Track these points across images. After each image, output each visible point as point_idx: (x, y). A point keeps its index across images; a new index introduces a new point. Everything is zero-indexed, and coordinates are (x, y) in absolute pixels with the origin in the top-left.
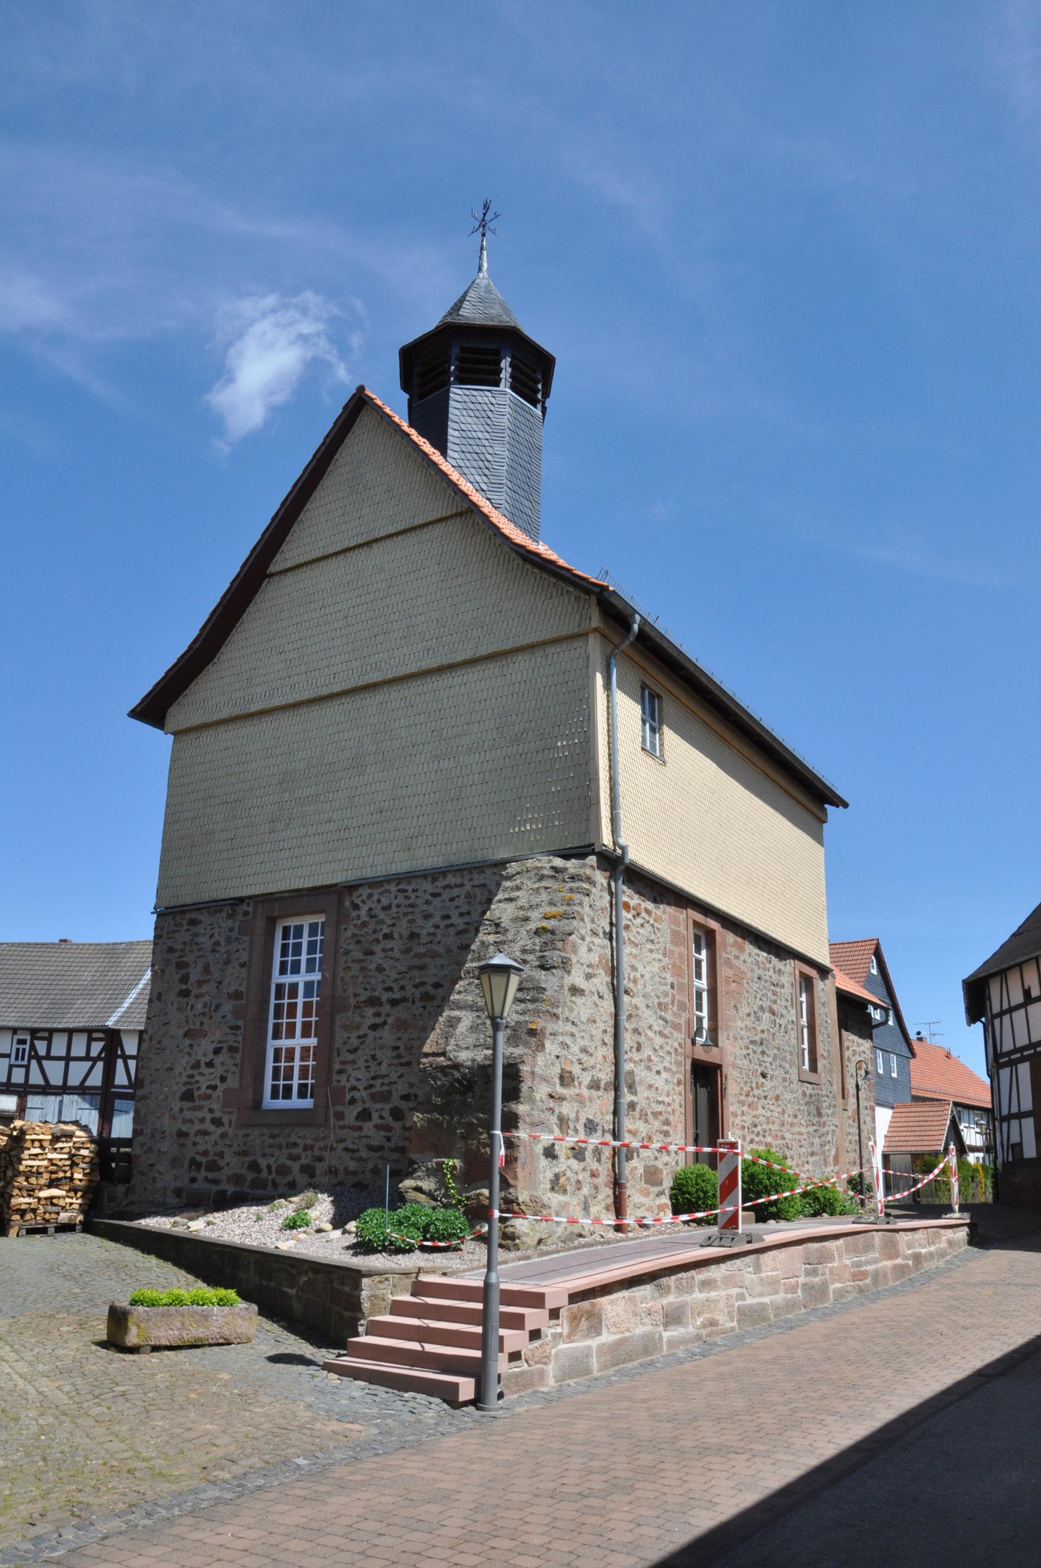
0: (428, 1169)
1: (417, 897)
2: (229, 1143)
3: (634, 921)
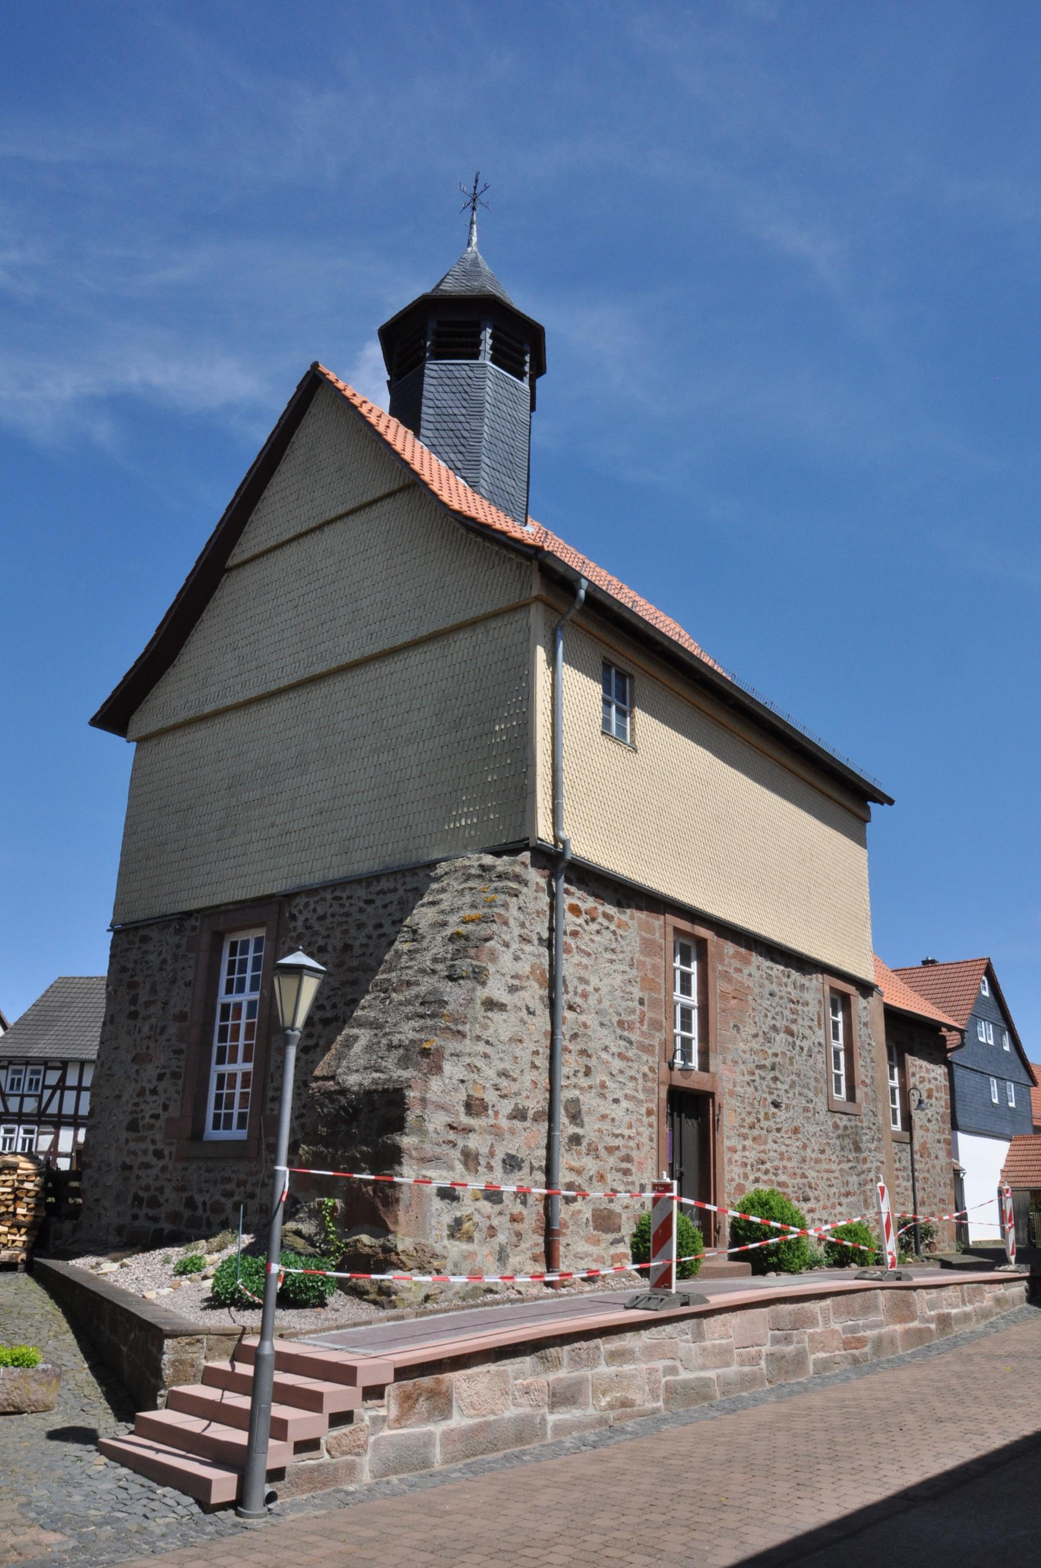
0: (310, 1210)
1: (351, 904)
2: (169, 1176)
3: (586, 927)
